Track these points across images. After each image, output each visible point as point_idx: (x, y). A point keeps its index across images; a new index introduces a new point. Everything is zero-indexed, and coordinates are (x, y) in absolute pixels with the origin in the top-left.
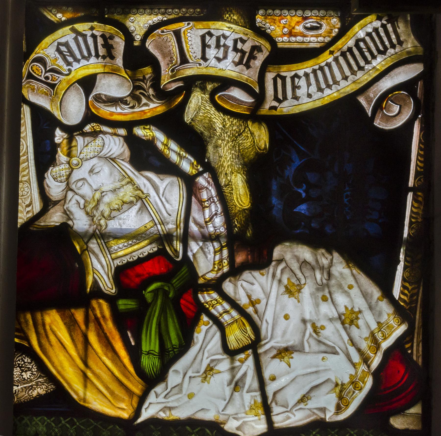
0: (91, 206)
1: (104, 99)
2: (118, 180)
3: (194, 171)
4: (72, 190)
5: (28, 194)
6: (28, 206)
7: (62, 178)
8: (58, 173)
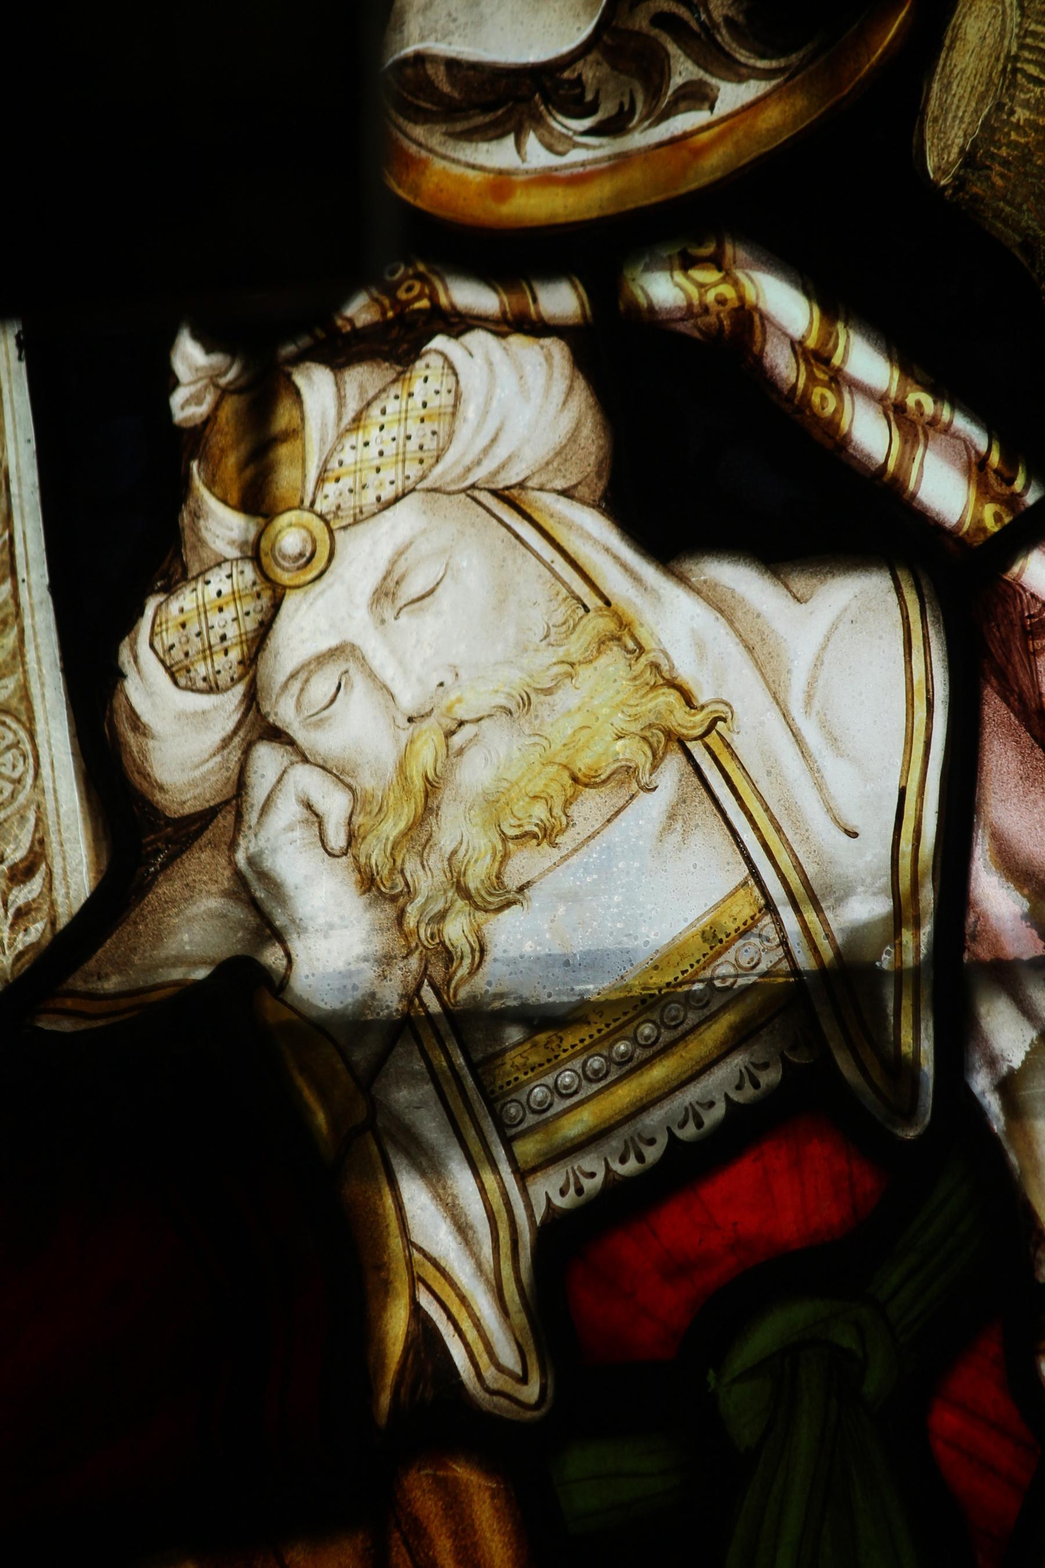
0: (392, 828)
1: (446, 88)
2: (541, 633)
3: (989, 511)
4: (277, 735)
5: (21, 798)
6: (22, 873)
7: (220, 660)
8: (193, 628)
